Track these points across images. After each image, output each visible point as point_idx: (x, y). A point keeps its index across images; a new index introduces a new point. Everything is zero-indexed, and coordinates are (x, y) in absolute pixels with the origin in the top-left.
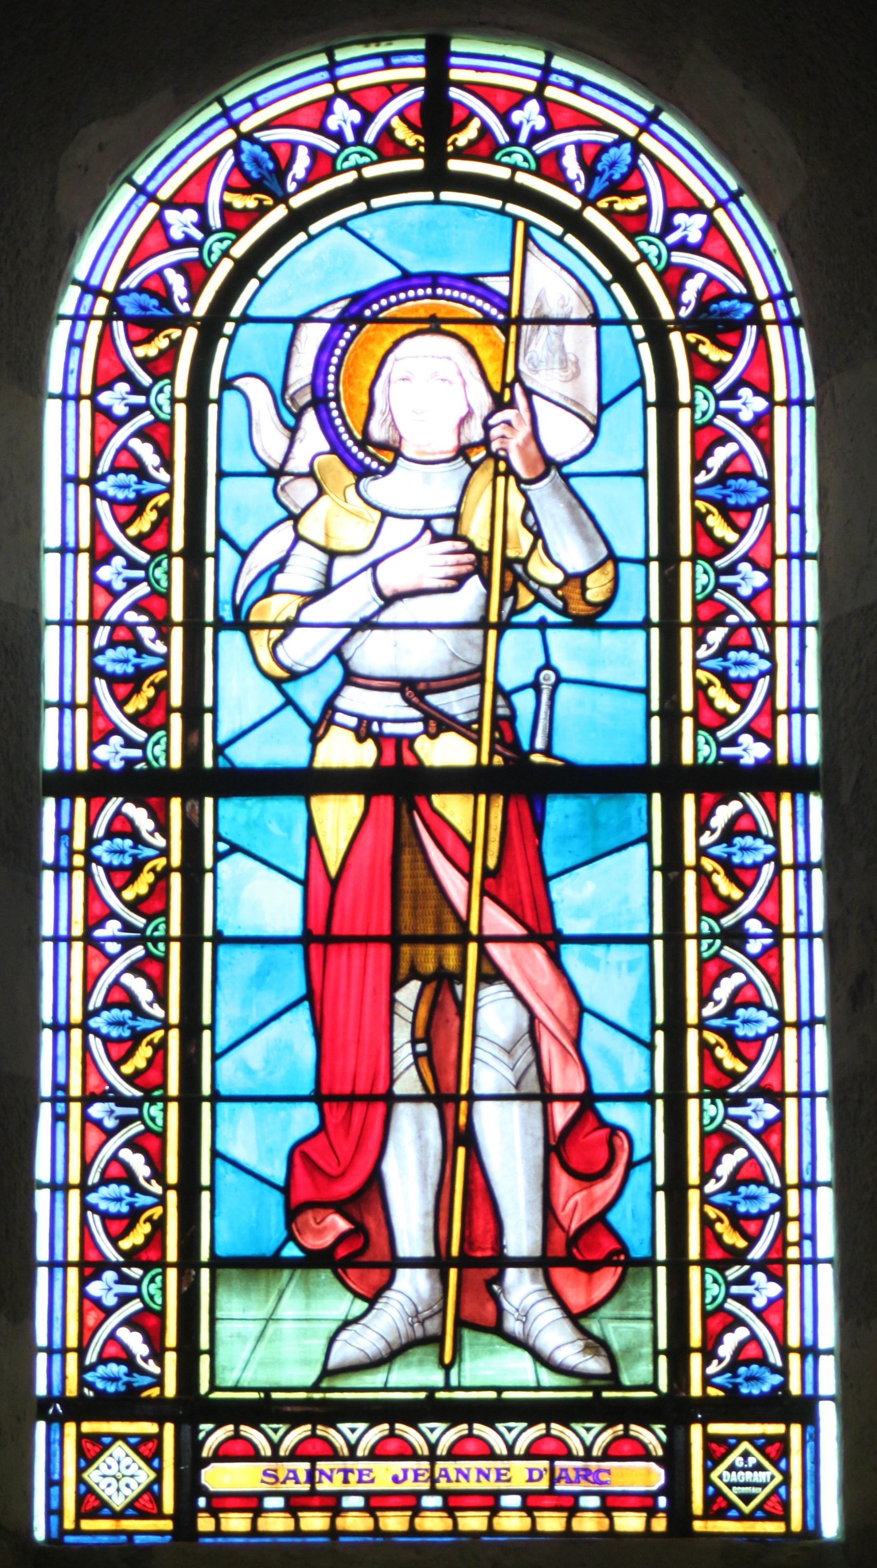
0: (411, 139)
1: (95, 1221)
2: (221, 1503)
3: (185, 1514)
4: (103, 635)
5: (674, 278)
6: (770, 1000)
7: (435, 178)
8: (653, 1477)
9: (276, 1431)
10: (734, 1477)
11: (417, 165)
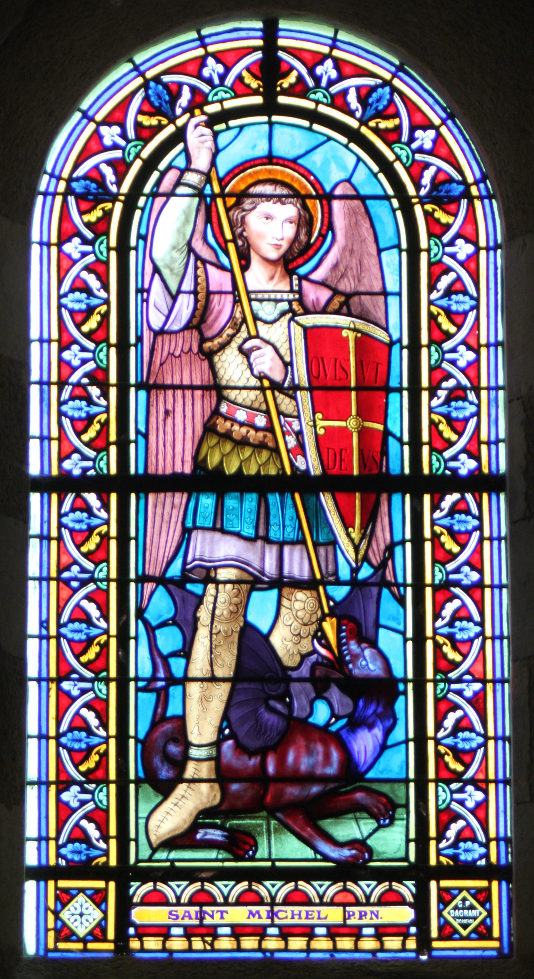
0: (254, 84)
1: (66, 423)
2: (143, 931)
3: (122, 937)
4: (67, 391)
5: (416, 170)
6: (478, 727)
7: (270, 108)
8: (404, 915)
9: (178, 886)
10: (457, 913)
11: (258, 100)
